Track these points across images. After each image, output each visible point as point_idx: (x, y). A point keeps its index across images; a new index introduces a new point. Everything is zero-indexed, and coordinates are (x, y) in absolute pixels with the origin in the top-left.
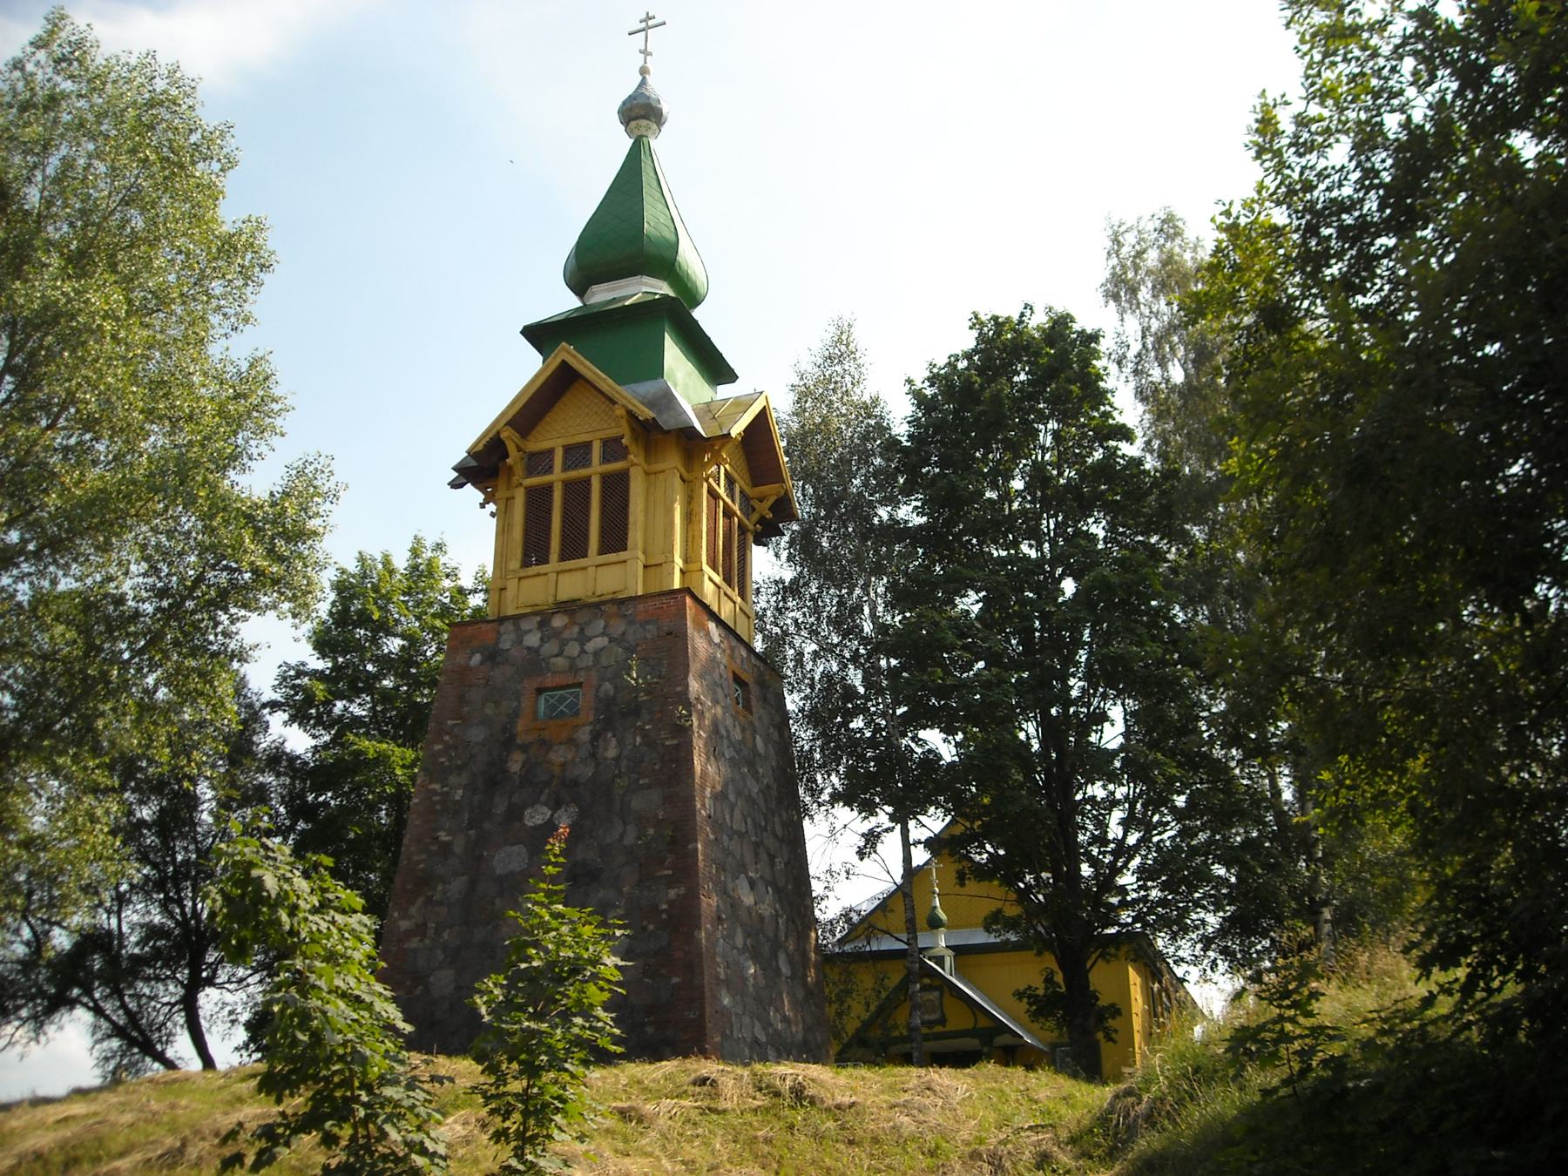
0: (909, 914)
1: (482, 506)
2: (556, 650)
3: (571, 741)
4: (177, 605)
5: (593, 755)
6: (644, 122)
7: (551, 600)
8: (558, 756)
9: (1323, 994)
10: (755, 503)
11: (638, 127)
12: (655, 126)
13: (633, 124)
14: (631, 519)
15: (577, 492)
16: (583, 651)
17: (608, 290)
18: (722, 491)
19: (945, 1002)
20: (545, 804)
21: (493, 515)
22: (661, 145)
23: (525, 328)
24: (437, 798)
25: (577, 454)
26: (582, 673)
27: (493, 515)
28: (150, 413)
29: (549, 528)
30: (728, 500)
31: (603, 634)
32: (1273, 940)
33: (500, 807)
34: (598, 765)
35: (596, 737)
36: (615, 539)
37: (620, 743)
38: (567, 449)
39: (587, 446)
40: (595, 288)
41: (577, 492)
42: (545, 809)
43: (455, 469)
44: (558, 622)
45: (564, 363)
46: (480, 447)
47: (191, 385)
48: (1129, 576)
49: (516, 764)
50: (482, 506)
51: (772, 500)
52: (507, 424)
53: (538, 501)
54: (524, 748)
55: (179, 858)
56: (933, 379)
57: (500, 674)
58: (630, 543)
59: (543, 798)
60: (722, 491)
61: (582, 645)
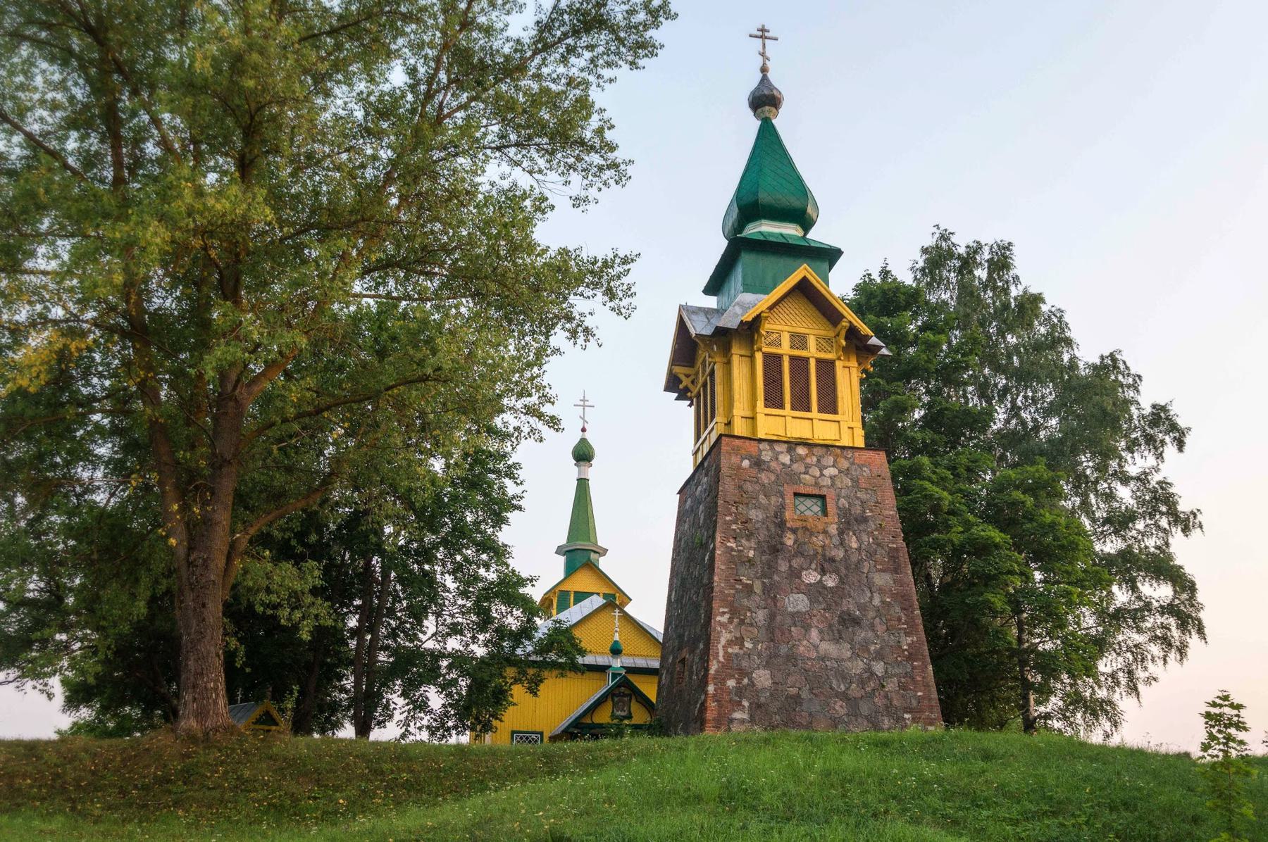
0: (702, 534)
2: (803, 470)
3: (825, 532)
4: (457, 370)
5: (842, 544)
6: (767, 108)
8: (819, 540)
9: (575, 343)
12: (774, 110)
13: (759, 110)
14: (840, 394)
16: (822, 475)
17: (771, 226)
22: (781, 122)
24: (734, 553)
26: (825, 489)
34: (846, 551)
35: (841, 533)
37: (858, 539)
40: (763, 221)
42: (815, 573)
43: (1110, 364)
48: (1097, 380)
49: (789, 540)
52: (863, 410)
54: (794, 531)
56: (1163, 484)
58: (840, 409)
59: (813, 566)
61: (821, 470)
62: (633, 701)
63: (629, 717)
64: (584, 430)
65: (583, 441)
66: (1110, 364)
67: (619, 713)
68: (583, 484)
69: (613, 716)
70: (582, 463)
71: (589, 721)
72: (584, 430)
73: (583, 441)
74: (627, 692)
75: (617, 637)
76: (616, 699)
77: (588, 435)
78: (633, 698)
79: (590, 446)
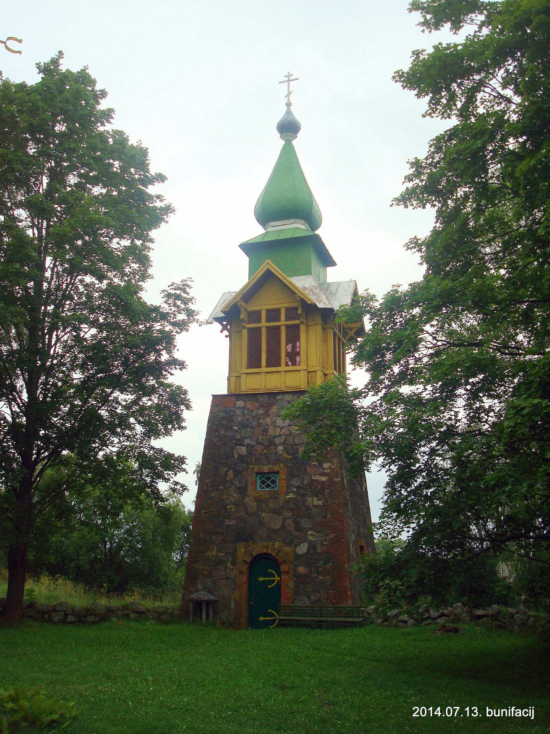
1: (221, 332)
7: (263, 387)
10: (348, 331)
15: (274, 332)
18: (337, 331)
21: (226, 336)
23: (241, 244)
25: (273, 314)
27: (226, 336)
29: (260, 348)
30: (339, 334)
32: (48, 533)
36: (293, 356)
38: (268, 311)
39: (278, 311)
41: (274, 332)
46: (227, 309)
47: (120, 326)
50: (221, 332)
51: (355, 330)
53: (254, 335)
55: (413, 497)
60: (337, 331)
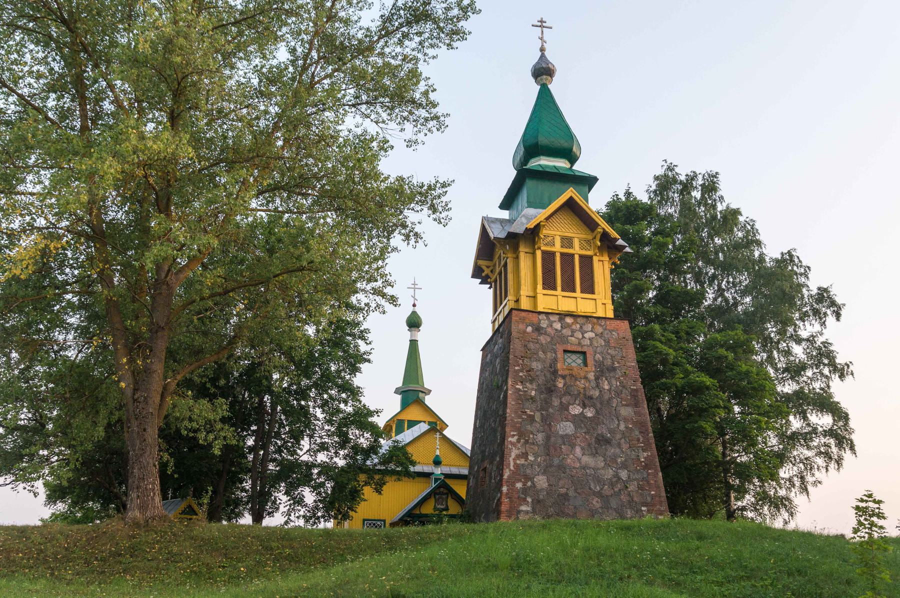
3: (586, 378)
5: (597, 386)
6: (544, 77)
8: (581, 384)
11: (541, 79)
16: (583, 337)
19: (449, 504)
20: (579, 405)
22: (554, 87)
28: (113, 203)
29: (562, 278)
31: (592, 331)
33: (556, 402)
35: (597, 378)
43: (788, 259)
44: (569, 320)
45: (571, 198)
49: (560, 384)
54: (564, 377)
57: (543, 339)
59: (577, 402)
62: (450, 498)
63: (447, 509)
64: (414, 305)
65: (414, 313)
66: (788, 259)
67: (439, 506)
68: (414, 344)
69: (435, 509)
70: (413, 329)
71: (418, 512)
72: (414, 305)
73: (414, 313)
74: (445, 491)
75: (438, 453)
76: (437, 497)
77: (417, 309)
78: (450, 495)
79: (419, 317)
